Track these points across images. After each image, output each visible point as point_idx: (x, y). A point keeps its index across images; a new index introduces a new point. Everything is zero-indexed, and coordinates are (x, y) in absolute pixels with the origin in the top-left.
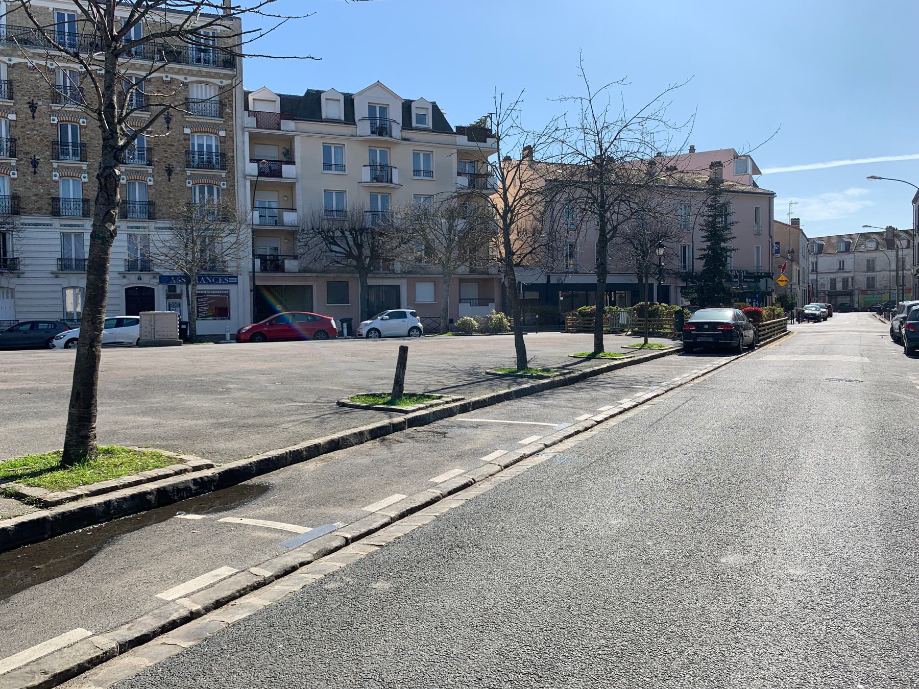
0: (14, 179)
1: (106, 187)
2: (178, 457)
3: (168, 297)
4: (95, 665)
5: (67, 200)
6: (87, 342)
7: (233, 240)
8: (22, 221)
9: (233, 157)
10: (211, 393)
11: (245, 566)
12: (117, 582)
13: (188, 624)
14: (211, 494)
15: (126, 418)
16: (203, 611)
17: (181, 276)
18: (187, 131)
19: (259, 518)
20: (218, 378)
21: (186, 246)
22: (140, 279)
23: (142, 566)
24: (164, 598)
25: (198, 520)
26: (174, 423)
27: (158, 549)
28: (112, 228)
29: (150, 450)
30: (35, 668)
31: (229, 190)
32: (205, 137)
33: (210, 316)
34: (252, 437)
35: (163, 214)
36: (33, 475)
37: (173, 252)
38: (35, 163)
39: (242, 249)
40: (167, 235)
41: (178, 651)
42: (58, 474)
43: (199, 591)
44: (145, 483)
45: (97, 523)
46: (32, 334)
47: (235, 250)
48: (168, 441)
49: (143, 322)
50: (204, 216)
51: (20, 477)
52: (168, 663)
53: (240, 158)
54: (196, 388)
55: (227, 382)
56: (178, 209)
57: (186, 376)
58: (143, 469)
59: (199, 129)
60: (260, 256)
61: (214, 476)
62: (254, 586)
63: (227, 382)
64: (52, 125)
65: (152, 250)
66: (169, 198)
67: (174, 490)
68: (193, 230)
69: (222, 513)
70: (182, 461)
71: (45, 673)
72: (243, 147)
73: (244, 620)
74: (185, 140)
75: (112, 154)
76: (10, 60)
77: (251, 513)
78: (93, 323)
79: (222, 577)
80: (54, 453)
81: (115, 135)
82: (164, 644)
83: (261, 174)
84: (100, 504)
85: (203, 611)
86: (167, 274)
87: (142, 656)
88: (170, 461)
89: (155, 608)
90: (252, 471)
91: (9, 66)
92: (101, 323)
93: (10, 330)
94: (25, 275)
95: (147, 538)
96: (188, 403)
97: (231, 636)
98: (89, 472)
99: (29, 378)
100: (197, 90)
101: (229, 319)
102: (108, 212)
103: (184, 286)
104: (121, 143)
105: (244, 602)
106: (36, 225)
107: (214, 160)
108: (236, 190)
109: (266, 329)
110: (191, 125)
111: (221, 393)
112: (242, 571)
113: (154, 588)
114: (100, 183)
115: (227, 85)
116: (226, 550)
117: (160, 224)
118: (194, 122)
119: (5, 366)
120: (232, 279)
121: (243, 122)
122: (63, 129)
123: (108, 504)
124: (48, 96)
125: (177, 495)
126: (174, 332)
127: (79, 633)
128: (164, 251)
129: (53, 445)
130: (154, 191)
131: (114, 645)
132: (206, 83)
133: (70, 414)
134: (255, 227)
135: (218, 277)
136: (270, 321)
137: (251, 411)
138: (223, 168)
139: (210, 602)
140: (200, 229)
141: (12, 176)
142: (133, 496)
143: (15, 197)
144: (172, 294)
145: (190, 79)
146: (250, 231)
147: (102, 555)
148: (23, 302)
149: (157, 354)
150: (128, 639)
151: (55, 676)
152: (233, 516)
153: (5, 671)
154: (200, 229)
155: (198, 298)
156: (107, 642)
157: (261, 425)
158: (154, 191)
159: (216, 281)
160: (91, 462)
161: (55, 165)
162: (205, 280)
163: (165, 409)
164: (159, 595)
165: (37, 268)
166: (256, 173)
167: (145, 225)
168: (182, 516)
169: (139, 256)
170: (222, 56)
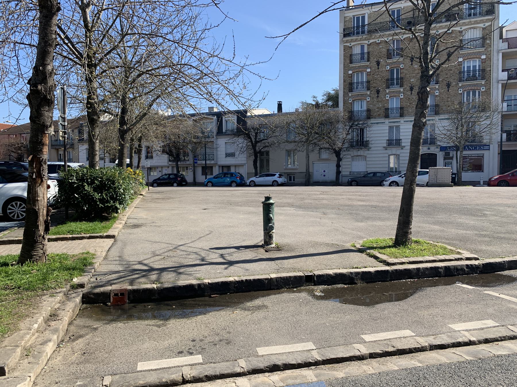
0: (368, 101)
1: (422, 99)
2: (457, 251)
3: (445, 159)
4: (417, 352)
5: (392, 109)
6: (409, 182)
7: (488, 122)
8: (371, 122)
9: (490, 70)
10: (474, 215)
11: (503, 323)
12: (426, 313)
13: (468, 347)
14: (477, 276)
15: (424, 225)
16: (477, 342)
17: (453, 146)
18: (461, 60)
19: (511, 296)
20: (478, 207)
21: (457, 128)
22: (429, 149)
23: (439, 307)
24: (453, 328)
25: (470, 289)
26: (453, 231)
27: (447, 300)
28: (424, 121)
29: (440, 244)
30: (389, 343)
31: (487, 91)
32: (472, 62)
33: (470, 170)
34: (505, 245)
35: (444, 111)
36: (381, 248)
37: (449, 132)
38: (378, 92)
39: (494, 128)
40: (446, 123)
41: (463, 360)
42: (393, 250)
43: (474, 330)
44: (438, 262)
45: (412, 279)
46: (374, 178)
47: (489, 128)
48: (449, 240)
49: (431, 173)
50: (470, 109)
51: (376, 248)
52: (458, 365)
53: (495, 70)
54: (464, 212)
55: (484, 210)
56: (454, 107)
57: (457, 205)
58: (436, 254)
59: (468, 57)
60: (506, 132)
61: (480, 265)
62: (511, 337)
63: (484, 210)
64: (387, 70)
65: (437, 131)
66: (448, 101)
67: (454, 269)
68: (462, 119)
69: (485, 288)
70: (459, 253)
71: (394, 347)
72: (498, 62)
73: (505, 355)
74: (459, 65)
75: (426, 80)
76: (484, 25)
77: (506, 292)
78: (412, 173)
79: (489, 326)
80: (390, 239)
81: (428, 69)
82: (455, 353)
83: (510, 78)
84: (414, 269)
85: (477, 342)
86: (445, 146)
87: (443, 355)
88: (452, 252)
89: (448, 332)
90: (505, 266)
91: (368, 45)
92: (416, 172)
93: (364, 177)
94: (371, 149)
95: (440, 293)
96: (460, 220)
97: (496, 362)
98: (408, 251)
99: (375, 200)
100: (471, 32)
101: (483, 171)
102: (423, 112)
103: (455, 152)
104: (431, 73)
105: (504, 345)
106: (377, 123)
107: (477, 75)
108: (491, 91)
109: (509, 178)
110: (463, 56)
111: (481, 216)
112: (502, 326)
113: (447, 321)
114: (419, 97)
115: (488, 26)
116: (490, 310)
117: (442, 117)
118: (466, 53)
119: (363, 194)
120: (486, 147)
121: (498, 47)
122: (392, 71)
123: (418, 269)
124: (385, 56)
125: (456, 272)
126: (448, 179)
127: (408, 333)
128: (444, 132)
129: (389, 235)
130: (439, 98)
131: (427, 345)
132: (474, 28)
133: (399, 219)
134: (503, 113)
135: (477, 146)
136: (512, 173)
137: (503, 230)
138: (483, 79)
139: (482, 338)
140: (466, 118)
141: (368, 100)
142: (431, 268)
143: (368, 110)
144: (447, 157)
145: (464, 28)
146: (500, 116)
147: (416, 295)
148: (370, 163)
149: (439, 191)
150: (434, 344)
151: (398, 350)
152: (493, 291)
153: (375, 340)
154: (466, 118)
155: (463, 159)
156: (424, 342)
157: (510, 239)
158: (439, 98)
159: (475, 149)
160: (409, 246)
161: (387, 91)
162: (468, 148)
163: (446, 222)
164: (450, 325)
165: (377, 145)
166: (506, 78)
167: (434, 118)
168: (460, 285)
169: (429, 136)
170: (485, 8)
